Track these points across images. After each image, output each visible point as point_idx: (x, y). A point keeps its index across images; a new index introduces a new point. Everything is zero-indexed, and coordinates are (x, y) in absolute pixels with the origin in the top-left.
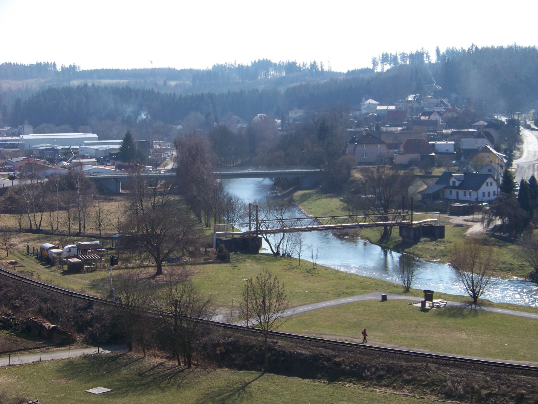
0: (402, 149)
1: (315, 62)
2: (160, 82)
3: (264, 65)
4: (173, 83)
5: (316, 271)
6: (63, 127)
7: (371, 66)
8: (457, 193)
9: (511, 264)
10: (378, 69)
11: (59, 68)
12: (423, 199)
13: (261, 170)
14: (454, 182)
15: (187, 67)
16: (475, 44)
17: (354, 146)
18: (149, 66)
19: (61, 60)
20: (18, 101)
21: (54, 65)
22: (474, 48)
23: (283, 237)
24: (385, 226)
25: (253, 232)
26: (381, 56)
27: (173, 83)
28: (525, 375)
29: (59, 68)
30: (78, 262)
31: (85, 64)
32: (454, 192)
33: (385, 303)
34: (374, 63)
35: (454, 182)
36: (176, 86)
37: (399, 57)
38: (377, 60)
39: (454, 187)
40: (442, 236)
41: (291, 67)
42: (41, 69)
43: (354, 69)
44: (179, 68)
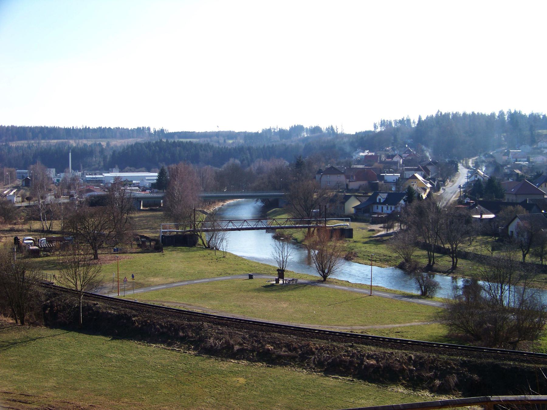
0: (354, 178)
1: (332, 126)
2: (221, 140)
3: (297, 129)
4: (231, 141)
5: (225, 260)
6: (140, 169)
7: (373, 129)
8: (382, 207)
9: (390, 256)
10: (378, 130)
11: (152, 131)
12: (356, 212)
13: (271, 196)
14: (380, 199)
15: (243, 130)
16: (441, 111)
17: (320, 176)
18: (217, 130)
19: (155, 125)
20: (114, 152)
21: (149, 129)
22: (439, 113)
23: (213, 235)
24: (309, 228)
25: (192, 231)
26: (380, 122)
27: (231, 141)
28: (281, 333)
29: (152, 131)
30: (36, 249)
31: (171, 128)
32: (380, 207)
33: (251, 281)
34: (375, 127)
35: (380, 199)
36: (233, 143)
37: (393, 123)
38: (377, 125)
39: (380, 203)
40: (351, 236)
41: (316, 130)
42: (140, 131)
43: (360, 131)
44: (237, 131)
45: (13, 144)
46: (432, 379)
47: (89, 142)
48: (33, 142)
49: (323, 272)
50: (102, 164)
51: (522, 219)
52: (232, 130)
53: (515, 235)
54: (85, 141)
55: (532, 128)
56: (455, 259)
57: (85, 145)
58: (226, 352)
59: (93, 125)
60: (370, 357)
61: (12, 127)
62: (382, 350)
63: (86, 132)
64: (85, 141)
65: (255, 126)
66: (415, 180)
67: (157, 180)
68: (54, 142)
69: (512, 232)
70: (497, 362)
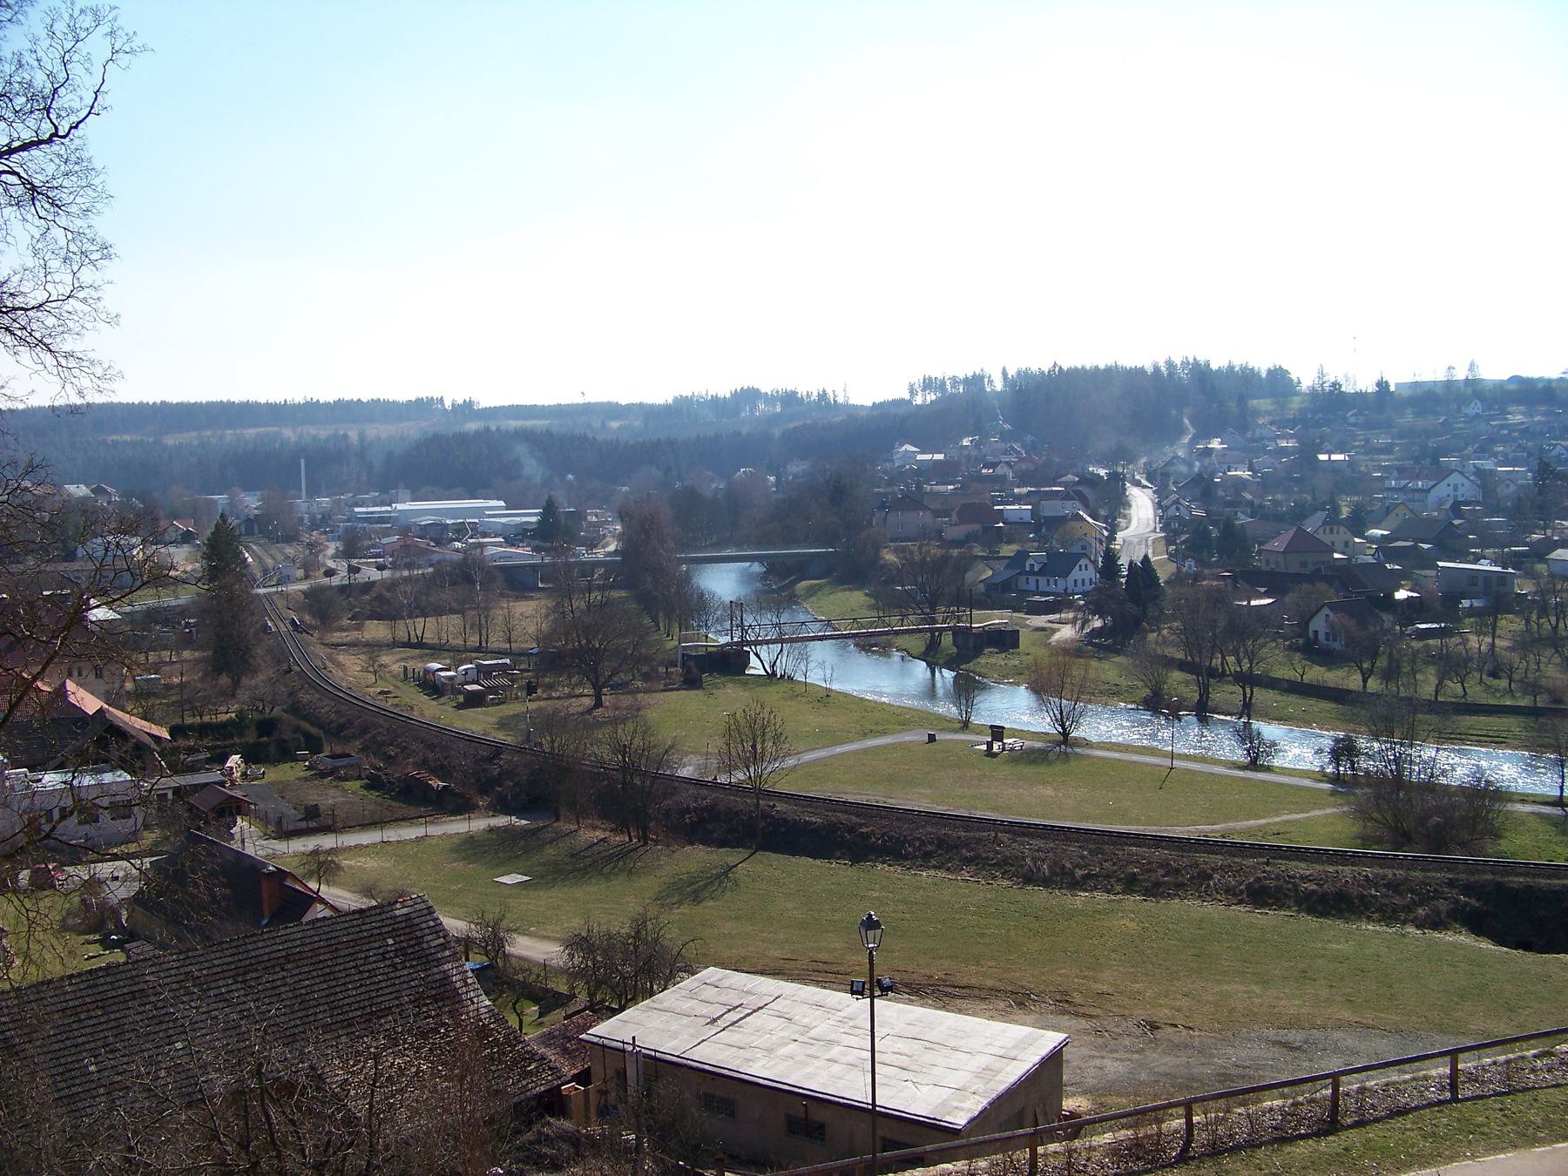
2: (597, 424)
4: (615, 424)
7: (907, 397)
10: (919, 400)
11: (448, 404)
14: (1032, 566)
19: (452, 394)
24: (932, 631)
27: (615, 424)
29: (448, 404)
31: (488, 397)
32: (1032, 579)
34: (912, 391)
35: (1032, 566)
39: (1032, 573)
41: (790, 398)
42: (423, 407)
45: (169, 441)
46: (1409, 909)
47: (324, 433)
48: (209, 433)
49: (1063, 726)
50: (364, 477)
51: (1332, 607)
52: (614, 399)
53: (1321, 636)
54: (313, 430)
55: (1242, 400)
56: (1248, 690)
57: (315, 438)
58: (1065, 879)
59: (327, 395)
60: (1304, 878)
61: (163, 403)
62: (1318, 867)
63: (310, 411)
64: (313, 430)
65: (659, 393)
66: (1080, 524)
67: (539, 522)
68: (251, 432)
69: (1316, 632)
70: (1499, 879)
